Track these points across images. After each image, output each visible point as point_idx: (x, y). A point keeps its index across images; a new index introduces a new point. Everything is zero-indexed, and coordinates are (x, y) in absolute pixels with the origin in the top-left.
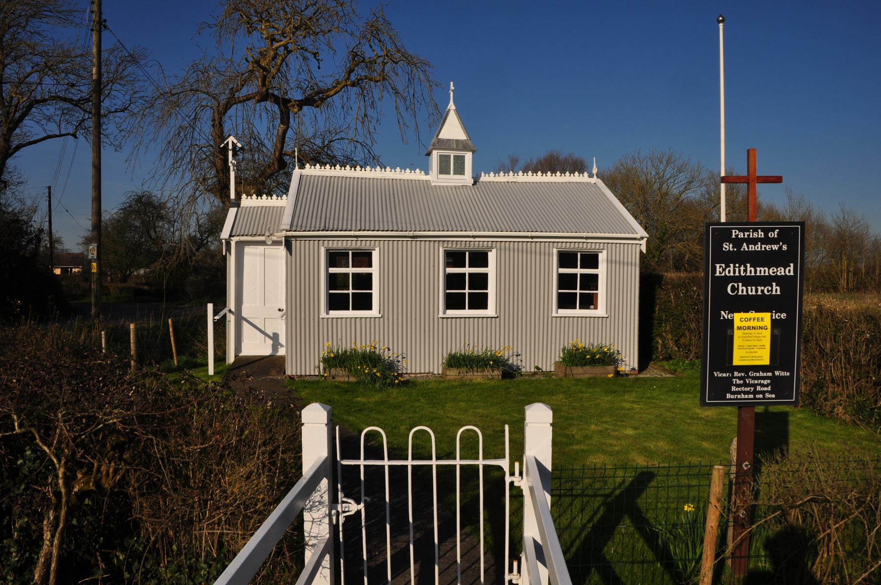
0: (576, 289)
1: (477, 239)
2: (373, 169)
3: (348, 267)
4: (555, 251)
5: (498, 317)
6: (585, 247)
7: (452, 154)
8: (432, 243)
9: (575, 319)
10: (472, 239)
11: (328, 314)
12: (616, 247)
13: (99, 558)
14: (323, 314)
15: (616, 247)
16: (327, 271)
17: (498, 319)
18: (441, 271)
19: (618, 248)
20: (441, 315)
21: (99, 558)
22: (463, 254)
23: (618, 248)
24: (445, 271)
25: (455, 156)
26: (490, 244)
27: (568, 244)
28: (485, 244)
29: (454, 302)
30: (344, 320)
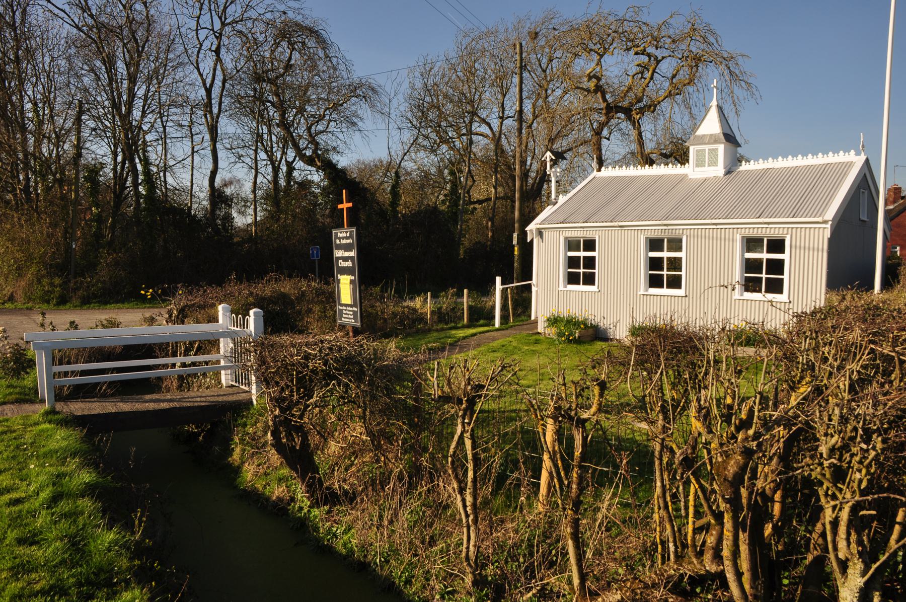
0: (762, 273)
1: (669, 227)
2: (766, 161)
3: (580, 251)
4: (738, 238)
5: (686, 296)
6: (768, 232)
7: (707, 147)
8: (808, 230)
9: (757, 302)
10: (766, 226)
11: (742, 295)
12: (801, 232)
13: (876, 496)
14: (561, 288)
15: (801, 232)
16: (743, 255)
17: (687, 298)
18: (642, 255)
19: (803, 233)
20: (642, 292)
21: (876, 496)
22: (761, 240)
23: (803, 233)
24: (647, 255)
25: (709, 150)
26: (681, 231)
27: (747, 230)
28: (677, 231)
29: (655, 282)
30: (757, 302)
